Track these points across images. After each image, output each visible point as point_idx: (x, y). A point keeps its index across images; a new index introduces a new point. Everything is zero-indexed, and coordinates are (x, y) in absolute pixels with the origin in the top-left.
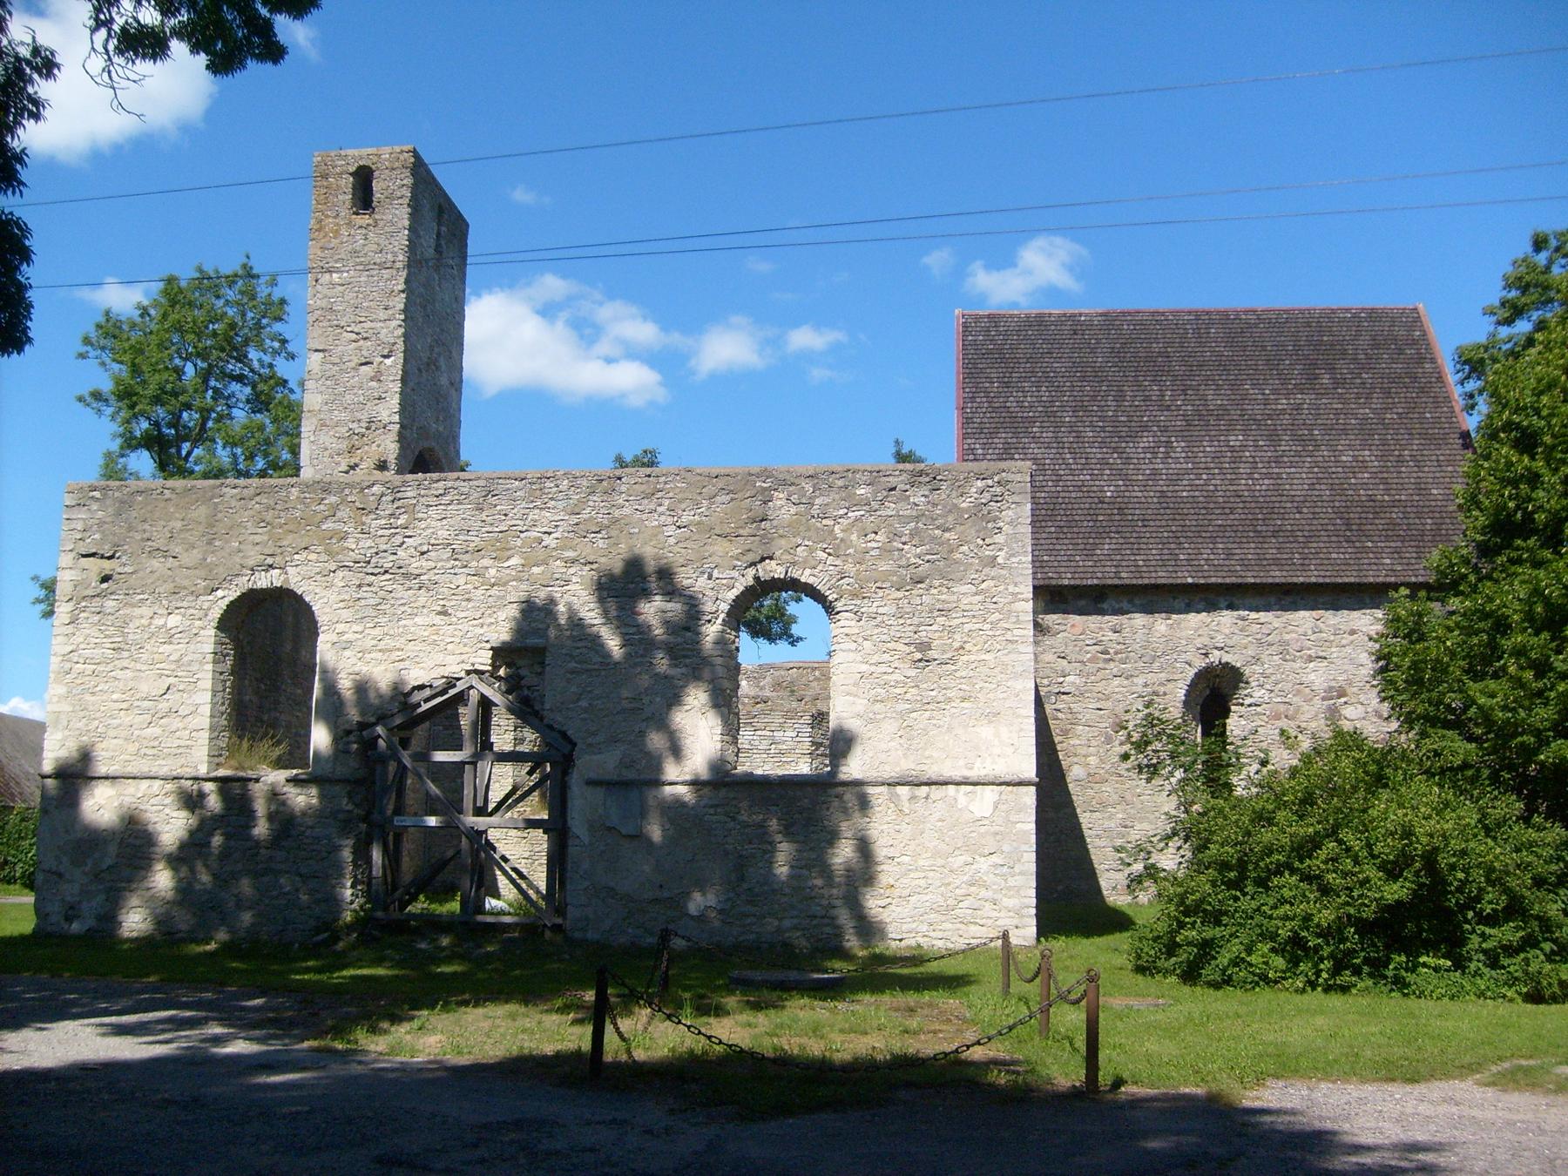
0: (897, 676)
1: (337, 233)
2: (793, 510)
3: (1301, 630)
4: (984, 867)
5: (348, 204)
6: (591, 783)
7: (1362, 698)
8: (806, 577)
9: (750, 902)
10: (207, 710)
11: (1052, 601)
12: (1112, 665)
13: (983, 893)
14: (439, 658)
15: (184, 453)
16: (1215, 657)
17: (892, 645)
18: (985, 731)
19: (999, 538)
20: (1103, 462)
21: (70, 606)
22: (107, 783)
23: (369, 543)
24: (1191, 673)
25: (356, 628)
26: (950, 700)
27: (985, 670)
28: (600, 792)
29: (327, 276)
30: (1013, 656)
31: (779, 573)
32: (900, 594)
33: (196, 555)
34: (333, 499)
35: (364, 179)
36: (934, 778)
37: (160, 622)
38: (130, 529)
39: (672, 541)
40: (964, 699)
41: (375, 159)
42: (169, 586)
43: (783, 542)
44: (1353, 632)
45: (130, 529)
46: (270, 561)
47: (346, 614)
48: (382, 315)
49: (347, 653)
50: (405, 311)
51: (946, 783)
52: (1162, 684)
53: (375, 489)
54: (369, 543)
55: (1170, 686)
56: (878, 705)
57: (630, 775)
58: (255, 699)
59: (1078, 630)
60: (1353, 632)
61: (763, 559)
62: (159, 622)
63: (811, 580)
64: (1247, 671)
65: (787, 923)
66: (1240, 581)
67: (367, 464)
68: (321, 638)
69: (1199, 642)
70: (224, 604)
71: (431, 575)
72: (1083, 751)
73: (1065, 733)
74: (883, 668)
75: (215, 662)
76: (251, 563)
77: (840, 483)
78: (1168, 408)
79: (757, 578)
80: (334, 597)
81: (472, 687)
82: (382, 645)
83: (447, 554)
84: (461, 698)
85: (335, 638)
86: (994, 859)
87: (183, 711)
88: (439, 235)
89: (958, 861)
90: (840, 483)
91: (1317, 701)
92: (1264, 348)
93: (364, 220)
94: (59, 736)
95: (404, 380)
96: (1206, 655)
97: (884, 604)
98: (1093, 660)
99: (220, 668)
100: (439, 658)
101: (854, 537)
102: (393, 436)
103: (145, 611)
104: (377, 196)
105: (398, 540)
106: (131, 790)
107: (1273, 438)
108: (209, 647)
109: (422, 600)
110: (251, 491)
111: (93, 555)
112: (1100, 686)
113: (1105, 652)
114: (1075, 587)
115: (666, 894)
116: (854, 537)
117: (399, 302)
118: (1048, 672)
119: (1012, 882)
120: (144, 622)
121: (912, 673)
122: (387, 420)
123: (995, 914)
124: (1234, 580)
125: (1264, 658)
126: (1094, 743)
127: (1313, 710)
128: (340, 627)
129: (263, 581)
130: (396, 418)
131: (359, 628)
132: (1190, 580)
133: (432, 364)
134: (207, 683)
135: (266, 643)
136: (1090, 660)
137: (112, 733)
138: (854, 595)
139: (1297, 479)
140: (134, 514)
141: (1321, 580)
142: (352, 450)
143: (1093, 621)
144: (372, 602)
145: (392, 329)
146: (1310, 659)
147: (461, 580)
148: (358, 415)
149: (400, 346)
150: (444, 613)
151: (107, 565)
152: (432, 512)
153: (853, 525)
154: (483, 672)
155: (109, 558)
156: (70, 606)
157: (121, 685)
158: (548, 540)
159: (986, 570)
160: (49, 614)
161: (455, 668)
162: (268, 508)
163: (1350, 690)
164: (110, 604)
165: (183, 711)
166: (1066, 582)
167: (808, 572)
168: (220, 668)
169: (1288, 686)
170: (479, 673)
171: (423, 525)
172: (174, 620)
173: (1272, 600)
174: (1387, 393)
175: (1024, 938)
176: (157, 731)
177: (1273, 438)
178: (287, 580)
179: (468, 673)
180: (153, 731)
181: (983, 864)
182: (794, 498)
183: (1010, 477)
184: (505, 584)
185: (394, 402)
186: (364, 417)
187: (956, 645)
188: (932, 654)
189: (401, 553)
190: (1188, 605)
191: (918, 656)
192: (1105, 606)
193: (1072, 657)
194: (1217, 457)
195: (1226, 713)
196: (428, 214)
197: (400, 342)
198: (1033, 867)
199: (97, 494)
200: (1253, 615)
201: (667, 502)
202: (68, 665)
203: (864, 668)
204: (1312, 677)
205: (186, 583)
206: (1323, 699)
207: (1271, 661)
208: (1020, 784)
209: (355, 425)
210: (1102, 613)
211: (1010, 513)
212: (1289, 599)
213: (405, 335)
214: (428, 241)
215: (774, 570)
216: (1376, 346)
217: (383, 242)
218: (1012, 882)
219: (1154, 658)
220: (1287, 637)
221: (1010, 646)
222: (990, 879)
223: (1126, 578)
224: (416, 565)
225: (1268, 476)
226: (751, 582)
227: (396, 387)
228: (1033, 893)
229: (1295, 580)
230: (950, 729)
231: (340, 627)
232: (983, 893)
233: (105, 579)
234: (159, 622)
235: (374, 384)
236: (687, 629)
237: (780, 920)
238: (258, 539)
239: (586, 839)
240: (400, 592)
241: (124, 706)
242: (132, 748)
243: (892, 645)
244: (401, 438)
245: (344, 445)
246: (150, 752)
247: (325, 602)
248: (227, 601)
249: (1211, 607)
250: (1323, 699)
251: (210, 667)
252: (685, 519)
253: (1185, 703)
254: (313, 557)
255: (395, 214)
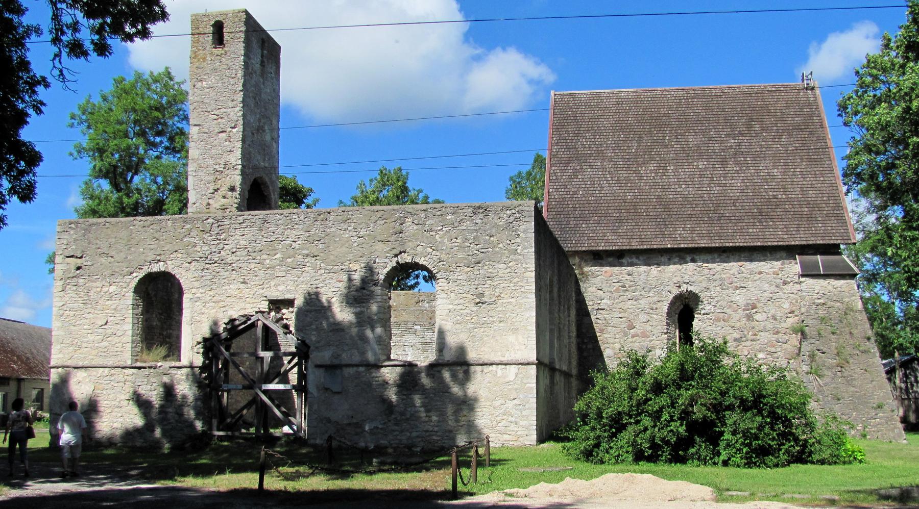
0: (467, 311)
1: (204, 59)
2: (415, 227)
3: (731, 272)
4: (511, 406)
5: (210, 42)
6: (318, 366)
7: (765, 309)
8: (422, 261)
9: (396, 424)
10: (130, 333)
11: (594, 259)
12: (627, 293)
13: (510, 419)
14: (242, 305)
15: (129, 178)
16: (684, 288)
17: (465, 295)
18: (511, 338)
19: (518, 240)
20: (628, 180)
21: (62, 282)
22: (83, 370)
23: (207, 248)
24: (671, 297)
25: (201, 291)
26: (493, 322)
27: (511, 307)
28: (322, 370)
29: (200, 83)
30: (525, 300)
31: (409, 259)
32: (469, 269)
33: (122, 255)
34: (188, 226)
35: (218, 28)
36: (486, 361)
37: (106, 289)
38: (89, 243)
39: (356, 244)
40: (500, 322)
41: (224, 16)
42: (110, 272)
43: (410, 244)
44: (760, 273)
45: (89, 243)
46: (158, 258)
47: (197, 284)
48: (231, 104)
49: (198, 304)
50: (243, 102)
51: (491, 364)
52: (655, 303)
53: (209, 221)
54: (207, 248)
55: (659, 304)
56: (458, 326)
57: (336, 362)
58: (159, 324)
59: (609, 274)
60: (760, 273)
61: (401, 253)
62: (105, 289)
63: (424, 263)
64: (702, 295)
65: (414, 434)
66: (697, 246)
67: (225, 188)
68: (185, 296)
69: (675, 280)
70: (136, 280)
71: (237, 264)
72: (612, 341)
73: (602, 331)
74: (460, 307)
75: (133, 309)
76: (149, 259)
77: (439, 213)
78: (666, 146)
79: (398, 262)
80: (190, 276)
81: (259, 320)
82: (214, 299)
83: (245, 252)
84: (254, 325)
85: (191, 296)
86: (515, 402)
87: (119, 334)
88: (262, 56)
89: (497, 403)
90: (439, 213)
91: (740, 311)
92: (723, 110)
93: (219, 51)
94: (59, 347)
95: (243, 141)
96: (679, 287)
97: (461, 275)
98: (617, 290)
99: (136, 312)
100: (242, 305)
101: (446, 241)
102: (238, 172)
103: (99, 284)
104: (226, 37)
105: (221, 246)
106: (95, 373)
107: (724, 162)
108: (130, 301)
109: (234, 276)
110: (149, 223)
111: (72, 256)
112: (621, 305)
113: (624, 286)
114: (606, 251)
115: (355, 421)
116: (446, 241)
117: (240, 97)
118: (592, 298)
119: (524, 413)
120: (99, 289)
121: (475, 309)
122: (235, 163)
123: (516, 429)
124: (693, 245)
125: (712, 288)
126: (617, 336)
127: (738, 317)
128: (194, 291)
129: (156, 268)
130: (240, 162)
131: (203, 291)
132: (669, 246)
133: (260, 129)
134: (130, 320)
135: (159, 299)
136: (615, 291)
137: (85, 345)
138: (446, 270)
139: (736, 185)
140: (91, 235)
141: (741, 244)
142: (216, 179)
143: (616, 270)
144: (209, 277)
145: (237, 112)
146: (737, 288)
147: (252, 266)
148: (219, 161)
149: (241, 122)
150: (244, 283)
151: (79, 262)
152: (237, 232)
153: (445, 234)
154: (264, 312)
155: (80, 258)
156: (62, 282)
157: (88, 321)
158: (294, 245)
159: (512, 257)
160: (52, 271)
161: (250, 311)
162: (157, 231)
163: (758, 305)
164: (81, 281)
165: (119, 334)
166: (601, 248)
167: (423, 259)
168: (136, 312)
169: (724, 303)
170: (263, 312)
171: (233, 238)
172: (112, 288)
173: (716, 256)
174: (790, 136)
175: (531, 441)
176: (105, 344)
177: (724, 162)
178: (167, 267)
179: (257, 312)
180: (105, 344)
181: (510, 404)
182: (416, 222)
183: (524, 208)
184: (274, 267)
185: (238, 153)
186: (222, 162)
187: (497, 294)
188: (485, 299)
189: (222, 253)
190: (669, 259)
191: (478, 300)
192: (624, 261)
193: (605, 289)
194: (691, 176)
195: (692, 318)
196: (255, 45)
197: (241, 119)
198: (535, 405)
199: (73, 226)
200: (705, 265)
201: (353, 225)
202: (61, 312)
203: (451, 307)
204: (738, 298)
205: (117, 270)
206: (744, 310)
207: (715, 290)
208: (528, 364)
209: (217, 167)
210: (621, 265)
211: (523, 227)
212: (725, 255)
213: (244, 116)
214: (256, 61)
215: (406, 258)
216: (788, 107)
217: (230, 64)
218: (524, 413)
219: (651, 289)
220: (724, 276)
221: (523, 295)
222: (513, 411)
223: (636, 246)
224: (231, 258)
225: (719, 185)
226: (395, 264)
227: (239, 145)
228: (535, 418)
229: (727, 245)
230: (494, 337)
231: (194, 291)
232: (510, 419)
233: (79, 268)
234: (105, 289)
235: (227, 143)
236: (364, 289)
237: (411, 433)
238: (152, 247)
239: (316, 394)
240: (223, 273)
241: (90, 331)
242: (94, 352)
243: (465, 295)
244: (243, 173)
245: (212, 178)
246: (103, 354)
247: (185, 278)
248: (138, 279)
249: (683, 261)
250: (744, 310)
251: (131, 311)
252: (362, 233)
253: (667, 313)
254: (180, 255)
255: (236, 46)
